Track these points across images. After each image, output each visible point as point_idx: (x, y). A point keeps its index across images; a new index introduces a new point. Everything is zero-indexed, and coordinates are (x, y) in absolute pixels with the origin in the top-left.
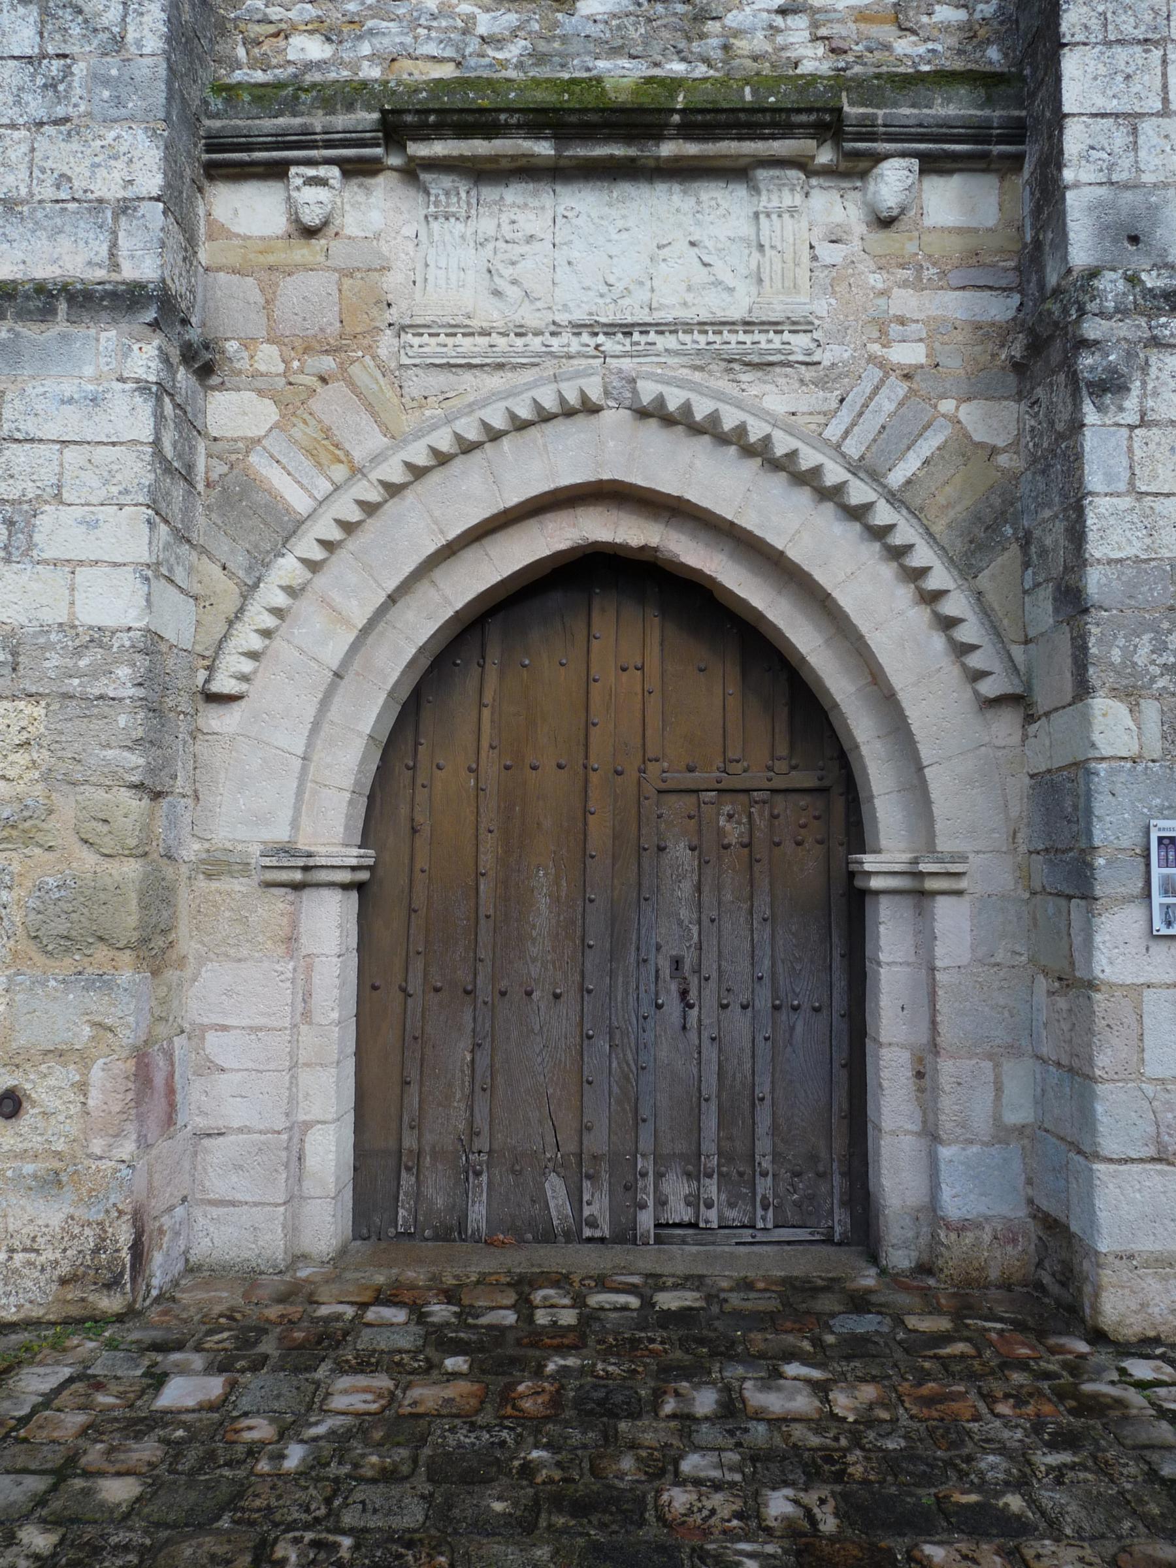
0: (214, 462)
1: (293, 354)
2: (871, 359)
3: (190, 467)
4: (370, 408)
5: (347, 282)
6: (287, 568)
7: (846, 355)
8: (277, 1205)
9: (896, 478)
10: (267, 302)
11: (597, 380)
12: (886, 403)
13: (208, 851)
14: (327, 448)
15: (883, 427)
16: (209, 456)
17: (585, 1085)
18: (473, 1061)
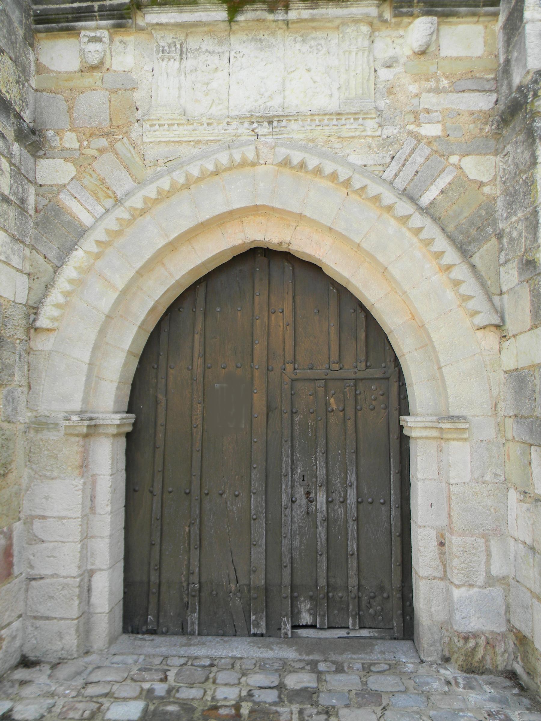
0: (40, 198)
1: (84, 137)
2: (410, 133)
3: (23, 201)
4: (127, 168)
5: (113, 97)
6: (78, 256)
7: (395, 132)
8: (73, 619)
9: (425, 200)
10: (70, 108)
11: (252, 147)
12: (419, 158)
13: (36, 417)
14: (103, 190)
15: (417, 172)
16: (37, 195)
17: (252, 546)
18: (190, 531)
